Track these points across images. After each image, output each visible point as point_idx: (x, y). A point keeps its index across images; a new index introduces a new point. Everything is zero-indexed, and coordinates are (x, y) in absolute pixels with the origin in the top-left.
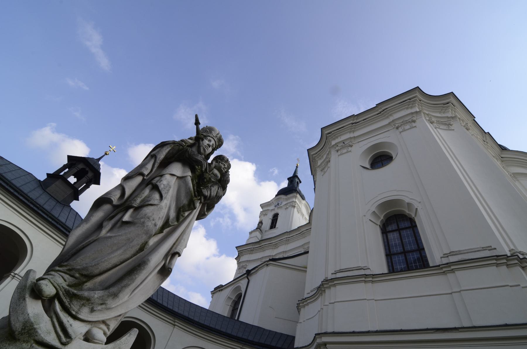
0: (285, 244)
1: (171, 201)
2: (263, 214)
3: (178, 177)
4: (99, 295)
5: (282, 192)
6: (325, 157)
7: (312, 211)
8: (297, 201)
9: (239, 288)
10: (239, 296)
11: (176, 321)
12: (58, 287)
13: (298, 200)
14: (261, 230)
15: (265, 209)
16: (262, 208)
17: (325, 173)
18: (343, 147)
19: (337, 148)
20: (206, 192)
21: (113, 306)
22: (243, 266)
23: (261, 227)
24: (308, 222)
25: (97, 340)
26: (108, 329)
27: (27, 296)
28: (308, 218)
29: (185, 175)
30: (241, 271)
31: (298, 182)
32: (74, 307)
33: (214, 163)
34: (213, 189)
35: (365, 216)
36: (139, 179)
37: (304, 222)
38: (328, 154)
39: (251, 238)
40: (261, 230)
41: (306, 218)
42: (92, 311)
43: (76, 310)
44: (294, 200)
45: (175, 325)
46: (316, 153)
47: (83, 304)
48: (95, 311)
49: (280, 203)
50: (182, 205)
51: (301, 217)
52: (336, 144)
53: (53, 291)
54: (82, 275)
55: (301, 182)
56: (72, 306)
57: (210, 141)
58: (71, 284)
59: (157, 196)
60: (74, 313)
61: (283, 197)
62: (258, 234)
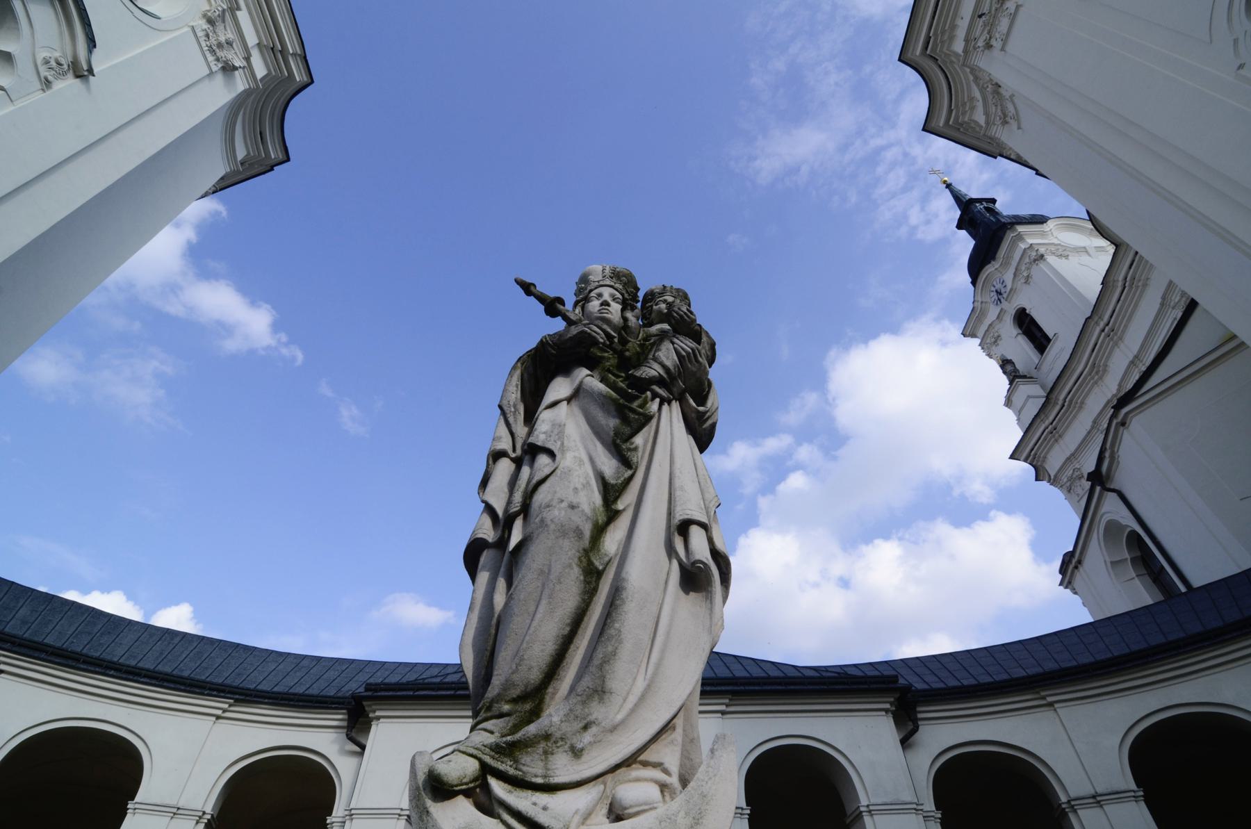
0: (1116, 344)
1: (586, 448)
2: (989, 346)
3: (569, 400)
4: (562, 713)
5: (976, 266)
6: (977, 94)
7: (1092, 218)
8: (1030, 241)
9: (1113, 529)
10: (1134, 540)
11: (1043, 694)
12: (475, 752)
13: (1031, 237)
14: (1025, 377)
15: (981, 332)
16: (973, 335)
17: (1017, 117)
18: (991, 27)
19: (981, 43)
20: (651, 370)
21: (620, 717)
22: (1071, 479)
23: (1016, 370)
24: (1111, 249)
25: (631, 807)
26: (666, 771)
27: (429, 803)
28: (1103, 243)
29: (577, 382)
30: (1080, 491)
31: (987, 209)
32: (533, 767)
33: (629, 315)
34: (662, 355)
35: (1241, 67)
36: (504, 468)
37: (1100, 255)
38: (976, 79)
39: (1020, 412)
40: (1025, 377)
41: (1100, 249)
42: (577, 753)
43: (540, 771)
44: (1022, 246)
45: (1051, 704)
46: (950, 111)
47: (546, 753)
48: (582, 750)
49: (999, 286)
50: (612, 433)
51: (1085, 259)
52: (967, 40)
53: (472, 766)
54: (514, 701)
55: (993, 201)
56: (524, 769)
57: (600, 295)
58: (505, 731)
59: (543, 460)
60: (539, 780)
61: (989, 269)
62: (1025, 389)
